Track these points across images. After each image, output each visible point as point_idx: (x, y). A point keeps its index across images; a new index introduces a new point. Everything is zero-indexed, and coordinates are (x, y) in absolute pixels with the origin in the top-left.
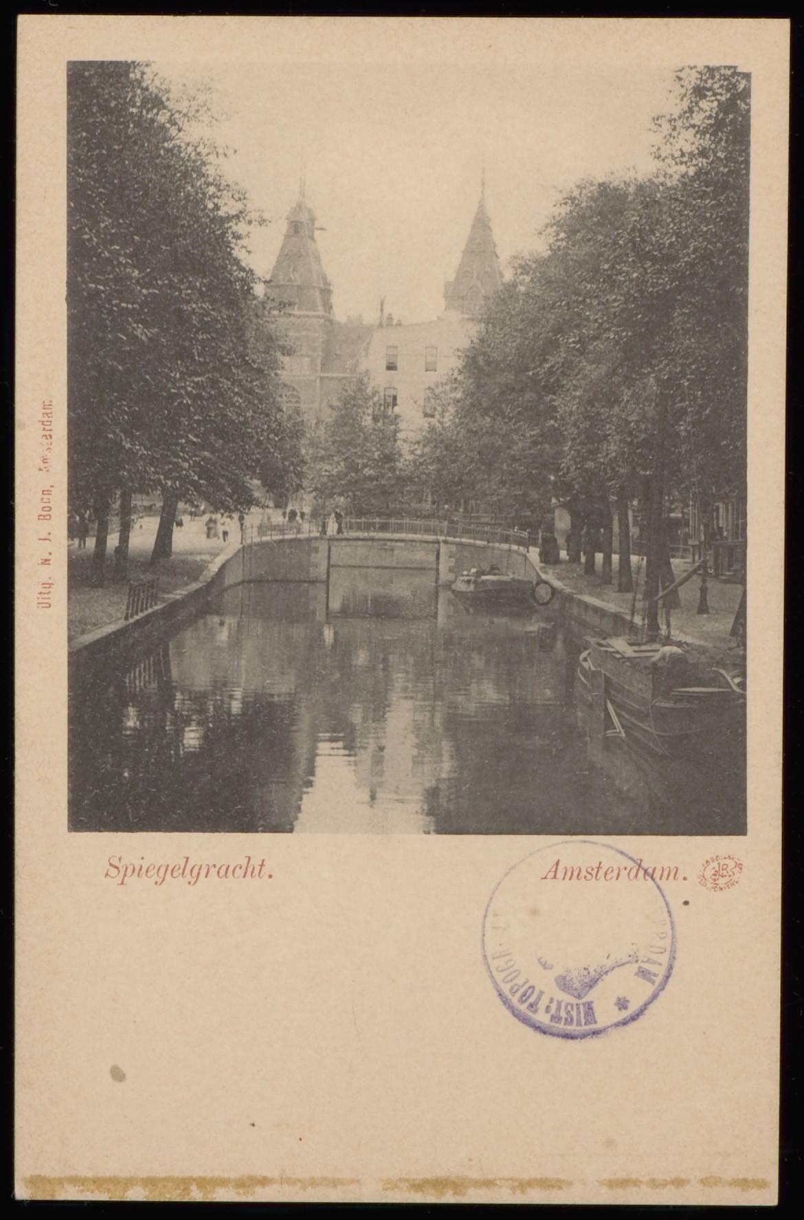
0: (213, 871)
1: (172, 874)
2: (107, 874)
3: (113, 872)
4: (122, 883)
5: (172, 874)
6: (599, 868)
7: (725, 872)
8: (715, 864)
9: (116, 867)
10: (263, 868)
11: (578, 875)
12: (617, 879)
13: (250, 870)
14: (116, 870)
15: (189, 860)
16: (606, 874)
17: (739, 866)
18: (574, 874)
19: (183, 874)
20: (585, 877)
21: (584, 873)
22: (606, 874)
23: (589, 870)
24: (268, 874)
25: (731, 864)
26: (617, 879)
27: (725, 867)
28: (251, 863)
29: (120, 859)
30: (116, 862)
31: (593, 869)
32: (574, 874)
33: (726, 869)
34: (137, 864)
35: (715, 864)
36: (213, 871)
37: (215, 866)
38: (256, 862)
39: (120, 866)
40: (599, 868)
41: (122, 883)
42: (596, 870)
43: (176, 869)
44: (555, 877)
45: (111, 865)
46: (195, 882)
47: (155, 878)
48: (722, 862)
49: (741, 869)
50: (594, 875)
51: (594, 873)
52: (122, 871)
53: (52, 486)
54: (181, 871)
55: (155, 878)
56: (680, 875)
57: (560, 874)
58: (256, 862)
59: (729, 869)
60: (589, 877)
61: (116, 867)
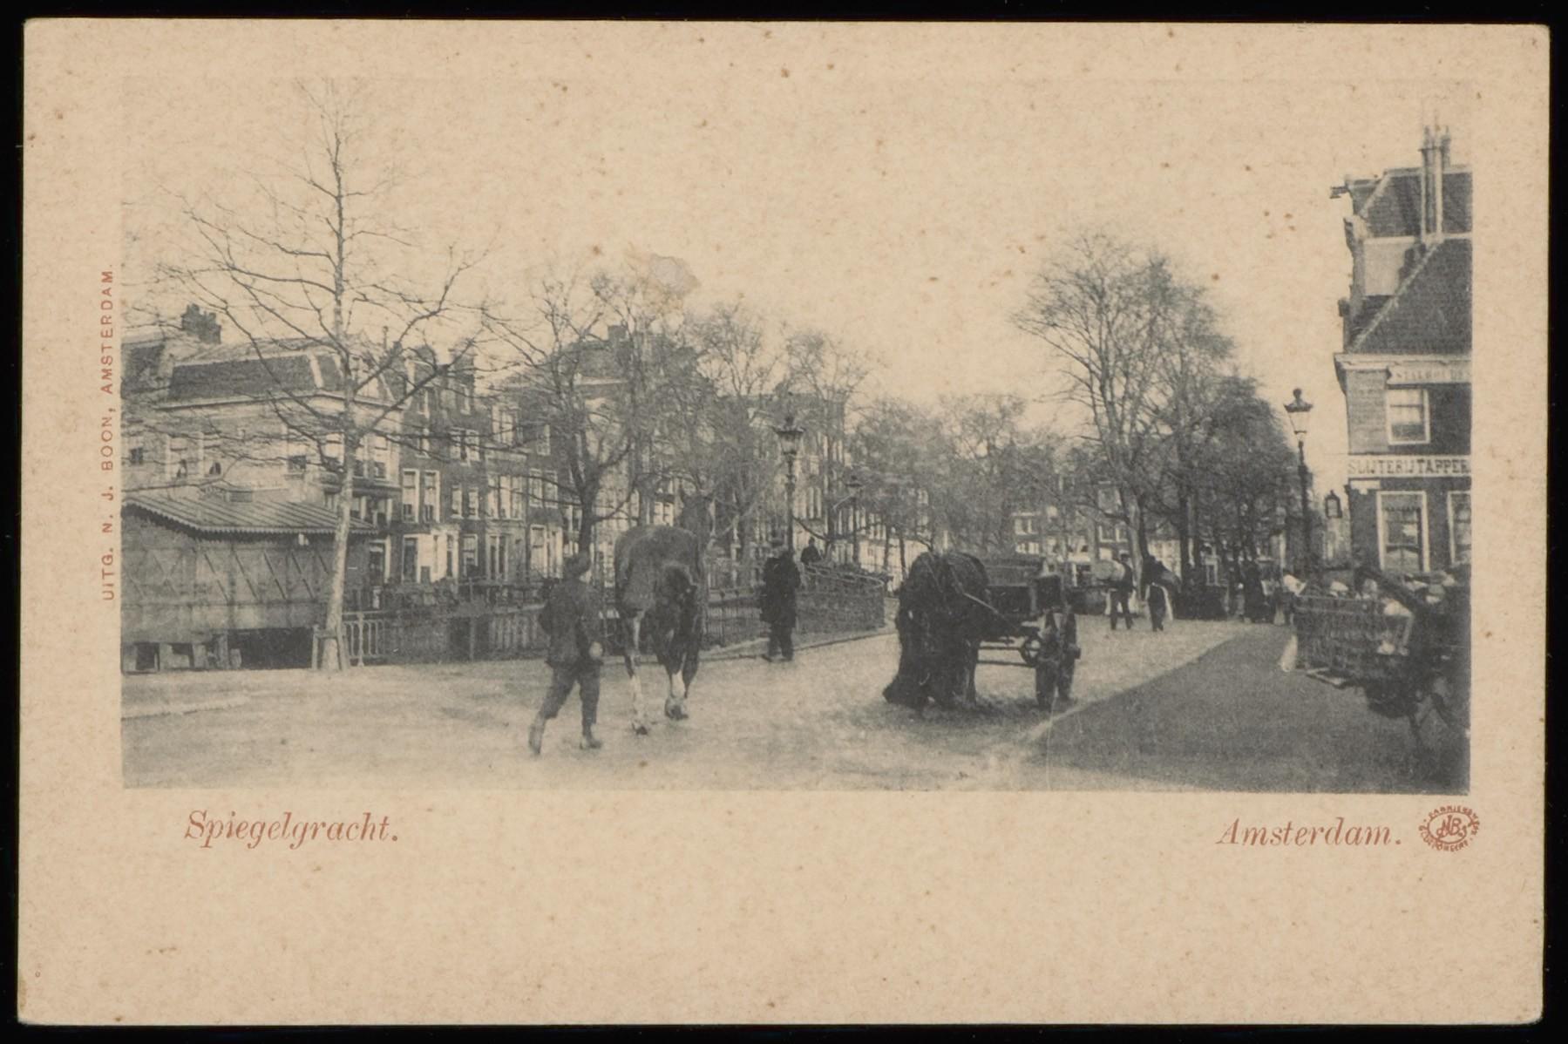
0: (322, 832)
1: (348, 835)
2: (188, 834)
3: (195, 830)
4: (206, 846)
5: (348, 835)
6: (1289, 829)
7: (1455, 829)
8: (1445, 817)
9: (199, 825)
10: (386, 827)
11: (1262, 839)
12: (1312, 842)
13: (369, 829)
14: (199, 829)
15: (292, 816)
16: (270, 832)
17: (1475, 824)
18: (1258, 837)
19: (284, 833)
20: (1272, 841)
21: (1269, 836)
22: (270, 832)
23: (1277, 832)
24: (391, 835)
25: (1466, 820)
26: (1312, 842)
27: (1456, 822)
28: (370, 822)
29: (204, 815)
30: (198, 818)
31: (1281, 831)
32: (1258, 837)
33: (1457, 825)
34: (226, 820)
35: (1445, 817)
36: (322, 832)
37: (324, 825)
38: (376, 820)
39: (204, 824)
40: (1289, 829)
41: (206, 846)
42: (1285, 832)
43: (275, 827)
44: (1233, 841)
45: (193, 822)
46: (257, 844)
47: (249, 840)
48: (1455, 815)
49: (1476, 828)
50: (1283, 839)
51: (1282, 835)
52: (207, 830)
53: (111, 488)
54: (281, 830)
55: (291, 840)
56: (1393, 837)
57: (1239, 838)
58: (376, 820)
59: (1461, 826)
60: (1276, 840)
61: (199, 825)
